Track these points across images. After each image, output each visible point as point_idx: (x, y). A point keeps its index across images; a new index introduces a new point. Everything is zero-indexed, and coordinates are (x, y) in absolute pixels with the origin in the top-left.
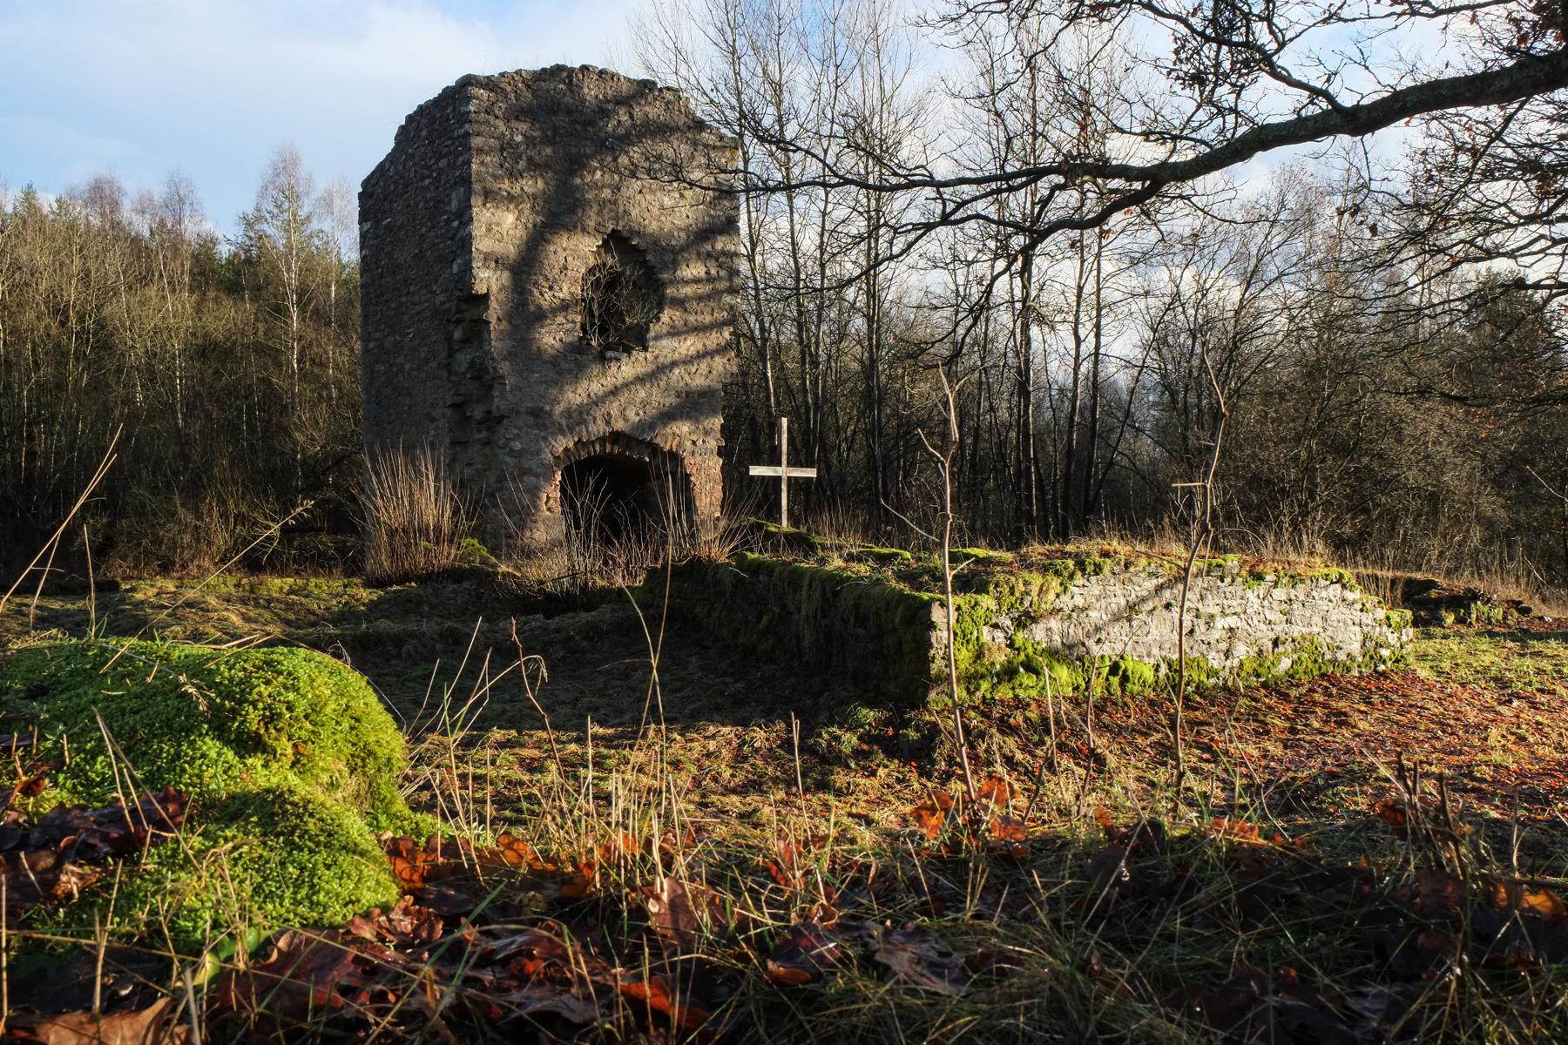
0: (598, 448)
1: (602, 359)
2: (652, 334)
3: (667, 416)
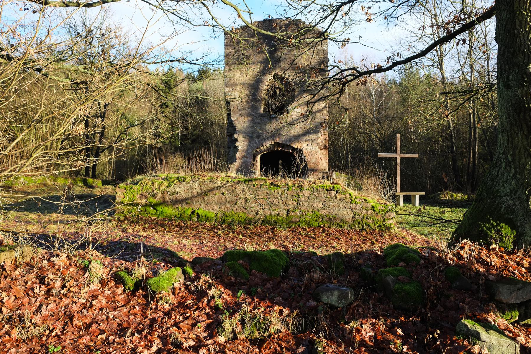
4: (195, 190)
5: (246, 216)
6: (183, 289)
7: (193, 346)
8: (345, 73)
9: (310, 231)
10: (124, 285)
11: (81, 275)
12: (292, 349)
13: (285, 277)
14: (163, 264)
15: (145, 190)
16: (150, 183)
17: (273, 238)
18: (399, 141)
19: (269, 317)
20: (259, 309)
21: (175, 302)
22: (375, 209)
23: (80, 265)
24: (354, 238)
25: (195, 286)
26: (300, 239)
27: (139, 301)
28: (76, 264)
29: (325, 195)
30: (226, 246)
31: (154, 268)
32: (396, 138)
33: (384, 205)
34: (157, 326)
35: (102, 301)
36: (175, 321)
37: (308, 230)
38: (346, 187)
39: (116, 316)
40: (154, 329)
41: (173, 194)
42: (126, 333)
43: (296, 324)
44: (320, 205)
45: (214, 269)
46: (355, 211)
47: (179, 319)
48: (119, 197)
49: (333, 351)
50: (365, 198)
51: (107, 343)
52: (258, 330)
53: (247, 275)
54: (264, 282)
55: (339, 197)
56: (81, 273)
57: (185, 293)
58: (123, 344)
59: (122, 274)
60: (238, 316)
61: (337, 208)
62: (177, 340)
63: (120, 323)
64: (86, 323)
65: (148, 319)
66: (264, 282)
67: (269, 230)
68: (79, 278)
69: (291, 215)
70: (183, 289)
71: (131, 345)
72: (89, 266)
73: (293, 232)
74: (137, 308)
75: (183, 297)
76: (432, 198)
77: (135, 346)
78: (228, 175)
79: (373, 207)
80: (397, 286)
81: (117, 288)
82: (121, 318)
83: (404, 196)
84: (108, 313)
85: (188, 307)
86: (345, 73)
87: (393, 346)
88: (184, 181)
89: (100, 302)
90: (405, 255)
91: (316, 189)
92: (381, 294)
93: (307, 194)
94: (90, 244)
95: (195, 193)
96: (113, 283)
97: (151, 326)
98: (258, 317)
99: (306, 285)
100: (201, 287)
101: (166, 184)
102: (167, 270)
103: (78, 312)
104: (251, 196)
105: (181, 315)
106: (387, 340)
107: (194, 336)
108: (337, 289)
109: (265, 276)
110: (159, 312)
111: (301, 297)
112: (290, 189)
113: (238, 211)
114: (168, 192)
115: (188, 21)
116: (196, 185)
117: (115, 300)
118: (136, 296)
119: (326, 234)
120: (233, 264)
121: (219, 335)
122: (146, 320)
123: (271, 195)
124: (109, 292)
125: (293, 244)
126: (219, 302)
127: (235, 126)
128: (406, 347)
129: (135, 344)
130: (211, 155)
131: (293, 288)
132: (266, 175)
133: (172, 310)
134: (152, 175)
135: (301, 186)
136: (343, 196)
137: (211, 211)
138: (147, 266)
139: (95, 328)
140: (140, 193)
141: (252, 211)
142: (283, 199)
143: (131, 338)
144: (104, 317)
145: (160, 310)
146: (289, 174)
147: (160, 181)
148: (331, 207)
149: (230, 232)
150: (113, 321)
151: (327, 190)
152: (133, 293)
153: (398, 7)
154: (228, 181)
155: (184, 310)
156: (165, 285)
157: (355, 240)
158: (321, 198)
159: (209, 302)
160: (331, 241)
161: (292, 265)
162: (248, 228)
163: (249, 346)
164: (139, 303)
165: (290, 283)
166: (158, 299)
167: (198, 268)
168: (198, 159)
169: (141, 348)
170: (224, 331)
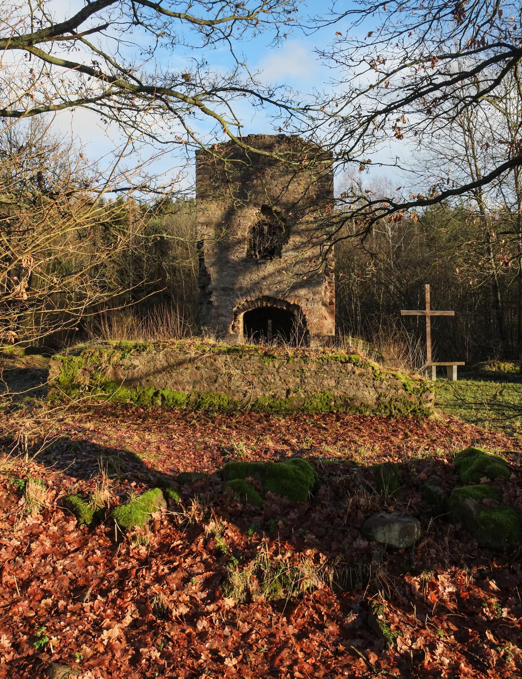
0: (259, 303)
1: (257, 264)
2: (284, 250)
3: (295, 287)
4: (158, 362)
5: (230, 398)
6: (165, 523)
7: (186, 615)
8: (377, 206)
9: (319, 419)
10: (78, 516)
11: (13, 502)
12: (338, 616)
13: (314, 501)
14: (134, 484)
15: (89, 363)
16: (97, 354)
17: (269, 430)
18: (429, 293)
19: (299, 567)
20: (283, 554)
21: (155, 544)
22: (408, 388)
23: (11, 486)
24: (380, 429)
25: (184, 517)
26: (305, 430)
27: (101, 541)
28: (5, 485)
29: (338, 369)
30: (206, 443)
31: (122, 491)
32: (423, 291)
33: (419, 383)
34: (130, 584)
35: (46, 543)
36: (157, 573)
37: (316, 417)
38: (367, 358)
39: (67, 567)
40: (126, 588)
41: (128, 369)
42: (84, 596)
43: (339, 575)
44: (333, 383)
45: (210, 491)
46: (380, 390)
47: (163, 570)
48: (53, 372)
49: (400, 620)
50: (394, 373)
51: (55, 613)
52: (284, 586)
53: (260, 499)
54: (286, 510)
55: (357, 372)
56: (13, 499)
57: (170, 529)
58: (79, 615)
59: (74, 499)
60: (252, 566)
61: (355, 387)
62: (162, 605)
63: (74, 577)
64: (22, 579)
65: (116, 572)
66: (286, 510)
67: (261, 417)
68: (10, 507)
69: (292, 397)
70: (165, 523)
71: (92, 614)
72: (24, 488)
73: (295, 420)
74: (98, 552)
75: (167, 536)
76: (474, 369)
77: (98, 616)
78: (204, 342)
79: (404, 385)
80: (482, 514)
81: (68, 522)
82: (74, 571)
83: (437, 367)
84: (54, 562)
85: (174, 551)
86: (377, 206)
87: (488, 609)
88: (143, 350)
89: (42, 544)
90: (488, 467)
91: (326, 361)
92: (459, 526)
93: (313, 367)
94: (25, 453)
95: (159, 366)
96: (60, 515)
97: (120, 584)
98: (283, 568)
99: (350, 515)
100: (193, 519)
101: (118, 354)
102: (142, 494)
103: (9, 562)
104: (237, 371)
105: (165, 564)
106: (475, 599)
107: (187, 598)
108: (397, 521)
109: (285, 500)
110: (132, 560)
111: (344, 533)
112: (291, 361)
113: (218, 392)
114: (121, 366)
115: (154, 138)
116: (161, 356)
117: (64, 541)
118: (95, 534)
119: (341, 423)
120: (239, 482)
121: (225, 596)
122: (113, 572)
123: (265, 370)
124: (56, 528)
125: (297, 438)
126: (221, 542)
127: (209, 275)
128: (506, 609)
129: (97, 613)
130: (176, 312)
131: (329, 518)
132: (257, 342)
133: (151, 556)
134: (99, 341)
135: (306, 356)
136: (363, 370)
137: (181, 391)
138: (110, 487)
139: (35, 587)
140: (83, 367)
141: (238, 392)
142: (280, 374)
143: (91, 603)
144: (49, 568)
145: (133, 557)
146: (289, 340)
147: (110, 351)
148: (347, 385)
149: (208, 422)
150: (62, 575)
151: (341, 362)
152: (92, 528)
153: (433, 119)
154: (205, 351)
155: (169, 556)
156: (140, 517)
157: (382, 431)
158: (333, 373)
159: (206, 542)
160: (350, 433)
161: (323, 482)
162: (232, 415)
163: (271, 612)
164: (100, 546)
165: (324, 511)
166: (130, 538)
167: (186, 489)
168: (159, 318)
169: (108, 620)
170: (232, 589)
